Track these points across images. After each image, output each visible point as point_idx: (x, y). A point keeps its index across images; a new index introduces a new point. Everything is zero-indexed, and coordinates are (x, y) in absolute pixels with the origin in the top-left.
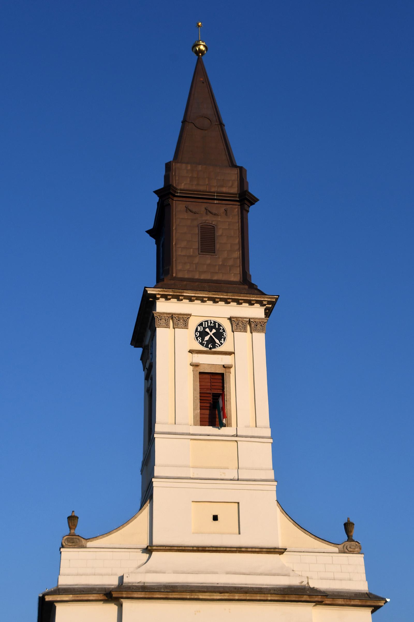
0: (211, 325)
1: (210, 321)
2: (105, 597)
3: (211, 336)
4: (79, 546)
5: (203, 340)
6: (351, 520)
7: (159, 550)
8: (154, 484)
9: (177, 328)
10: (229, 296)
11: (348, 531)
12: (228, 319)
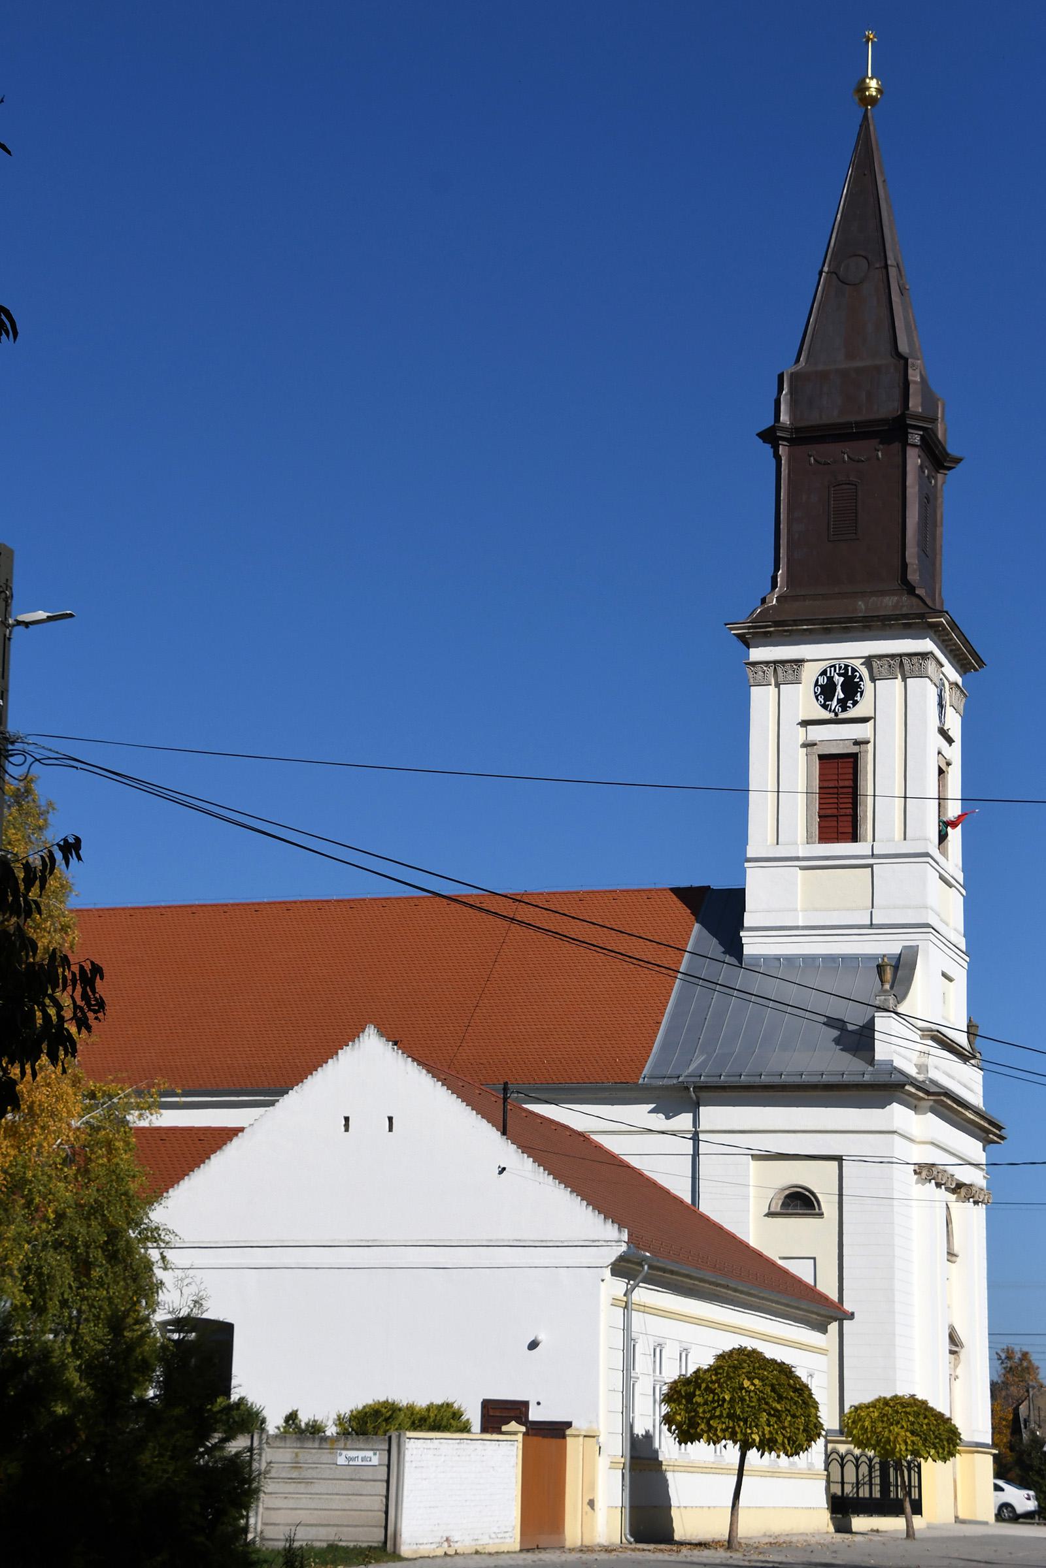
0: (841, 672)
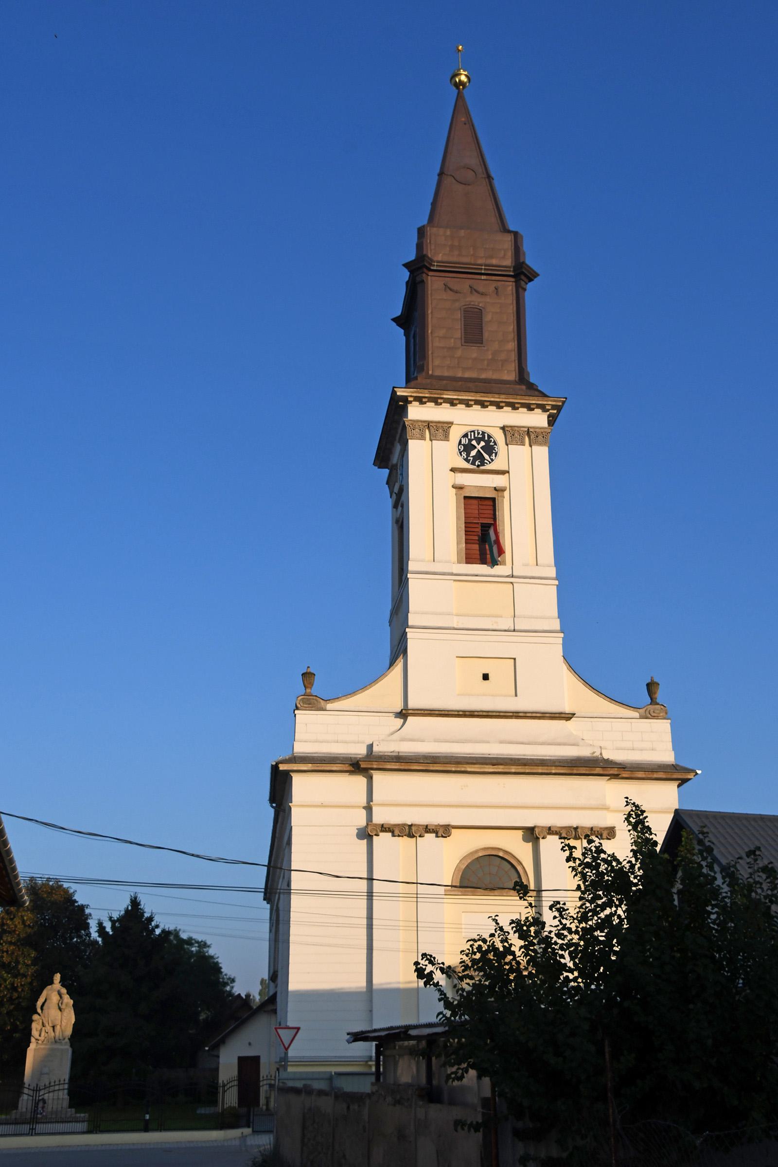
0: (479, 436)
1: (478, 431)
3: (479, 451)
5: (468, 455)
8: (409, 636)
9: (435, 440)
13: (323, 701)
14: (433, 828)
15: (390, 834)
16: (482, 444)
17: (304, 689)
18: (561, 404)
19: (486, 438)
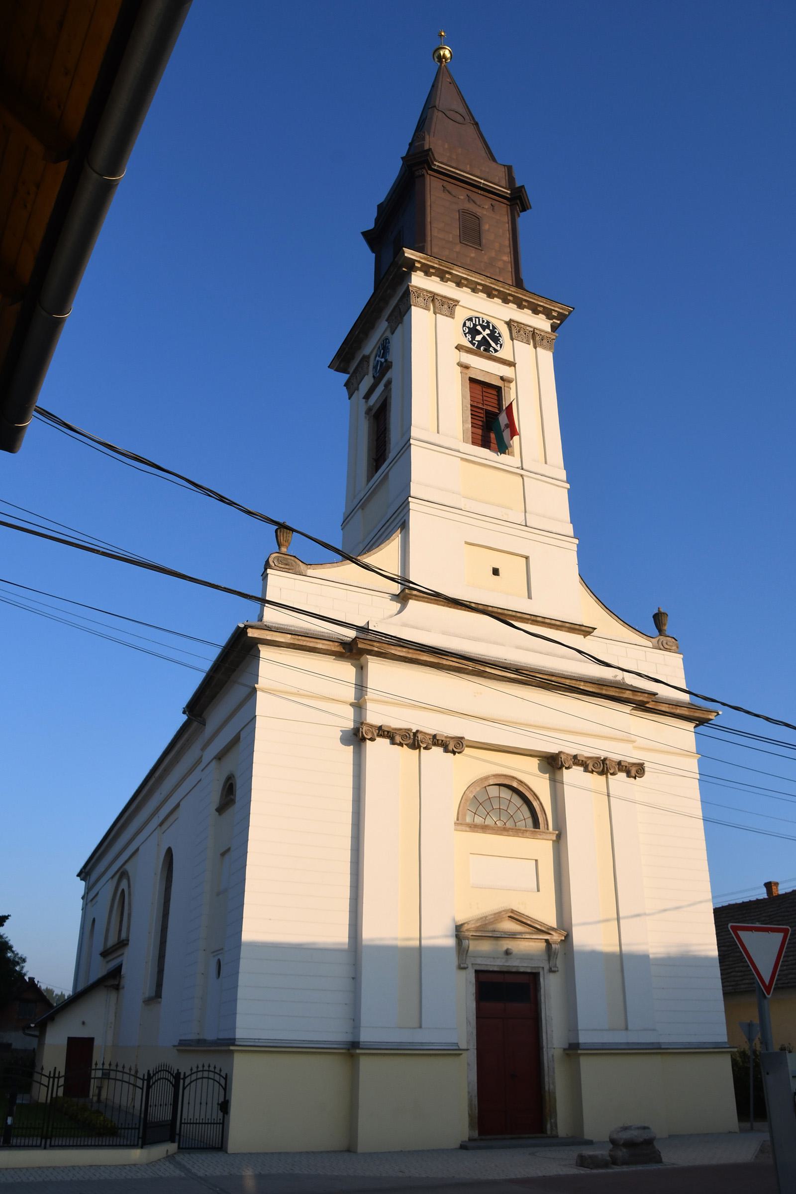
0: (484, 324)
1: (482, 319)
2: (342, 649)
3: (484, 337)
4: (295, 571)
5: (473, 338)
6: (662, 610)
7: (419, 598)
8: (412, 506)
9: (439, 313)
10: (512, 291)
11: (661, 622)
12: (505, 323)
13: (304, 565)
14: (443, 739)
15: (388, 741)
16: (487, 331)
17: (278, 547)
18: (567, 313)
19: (491, 328)
